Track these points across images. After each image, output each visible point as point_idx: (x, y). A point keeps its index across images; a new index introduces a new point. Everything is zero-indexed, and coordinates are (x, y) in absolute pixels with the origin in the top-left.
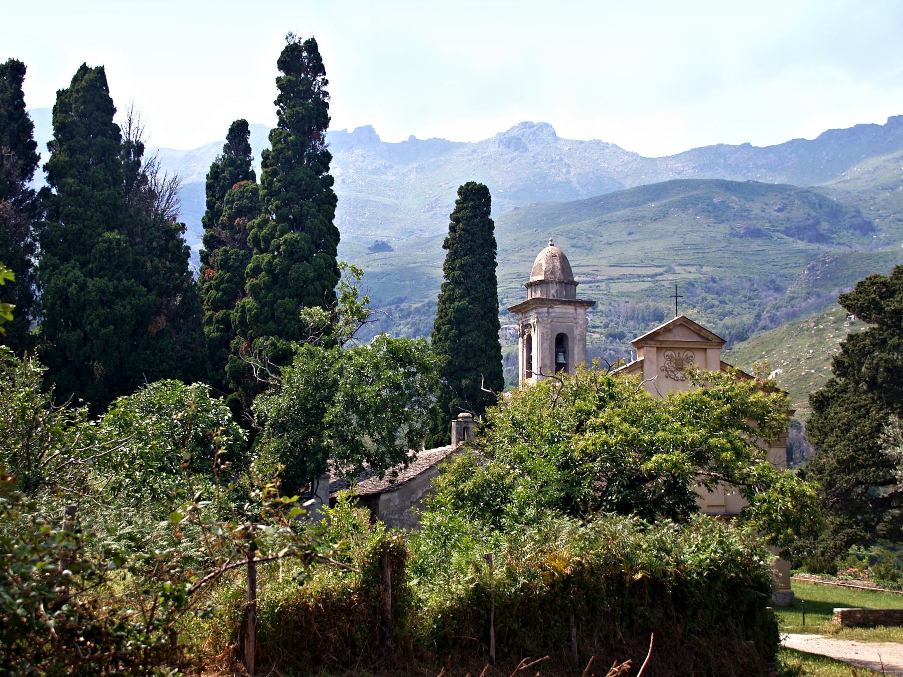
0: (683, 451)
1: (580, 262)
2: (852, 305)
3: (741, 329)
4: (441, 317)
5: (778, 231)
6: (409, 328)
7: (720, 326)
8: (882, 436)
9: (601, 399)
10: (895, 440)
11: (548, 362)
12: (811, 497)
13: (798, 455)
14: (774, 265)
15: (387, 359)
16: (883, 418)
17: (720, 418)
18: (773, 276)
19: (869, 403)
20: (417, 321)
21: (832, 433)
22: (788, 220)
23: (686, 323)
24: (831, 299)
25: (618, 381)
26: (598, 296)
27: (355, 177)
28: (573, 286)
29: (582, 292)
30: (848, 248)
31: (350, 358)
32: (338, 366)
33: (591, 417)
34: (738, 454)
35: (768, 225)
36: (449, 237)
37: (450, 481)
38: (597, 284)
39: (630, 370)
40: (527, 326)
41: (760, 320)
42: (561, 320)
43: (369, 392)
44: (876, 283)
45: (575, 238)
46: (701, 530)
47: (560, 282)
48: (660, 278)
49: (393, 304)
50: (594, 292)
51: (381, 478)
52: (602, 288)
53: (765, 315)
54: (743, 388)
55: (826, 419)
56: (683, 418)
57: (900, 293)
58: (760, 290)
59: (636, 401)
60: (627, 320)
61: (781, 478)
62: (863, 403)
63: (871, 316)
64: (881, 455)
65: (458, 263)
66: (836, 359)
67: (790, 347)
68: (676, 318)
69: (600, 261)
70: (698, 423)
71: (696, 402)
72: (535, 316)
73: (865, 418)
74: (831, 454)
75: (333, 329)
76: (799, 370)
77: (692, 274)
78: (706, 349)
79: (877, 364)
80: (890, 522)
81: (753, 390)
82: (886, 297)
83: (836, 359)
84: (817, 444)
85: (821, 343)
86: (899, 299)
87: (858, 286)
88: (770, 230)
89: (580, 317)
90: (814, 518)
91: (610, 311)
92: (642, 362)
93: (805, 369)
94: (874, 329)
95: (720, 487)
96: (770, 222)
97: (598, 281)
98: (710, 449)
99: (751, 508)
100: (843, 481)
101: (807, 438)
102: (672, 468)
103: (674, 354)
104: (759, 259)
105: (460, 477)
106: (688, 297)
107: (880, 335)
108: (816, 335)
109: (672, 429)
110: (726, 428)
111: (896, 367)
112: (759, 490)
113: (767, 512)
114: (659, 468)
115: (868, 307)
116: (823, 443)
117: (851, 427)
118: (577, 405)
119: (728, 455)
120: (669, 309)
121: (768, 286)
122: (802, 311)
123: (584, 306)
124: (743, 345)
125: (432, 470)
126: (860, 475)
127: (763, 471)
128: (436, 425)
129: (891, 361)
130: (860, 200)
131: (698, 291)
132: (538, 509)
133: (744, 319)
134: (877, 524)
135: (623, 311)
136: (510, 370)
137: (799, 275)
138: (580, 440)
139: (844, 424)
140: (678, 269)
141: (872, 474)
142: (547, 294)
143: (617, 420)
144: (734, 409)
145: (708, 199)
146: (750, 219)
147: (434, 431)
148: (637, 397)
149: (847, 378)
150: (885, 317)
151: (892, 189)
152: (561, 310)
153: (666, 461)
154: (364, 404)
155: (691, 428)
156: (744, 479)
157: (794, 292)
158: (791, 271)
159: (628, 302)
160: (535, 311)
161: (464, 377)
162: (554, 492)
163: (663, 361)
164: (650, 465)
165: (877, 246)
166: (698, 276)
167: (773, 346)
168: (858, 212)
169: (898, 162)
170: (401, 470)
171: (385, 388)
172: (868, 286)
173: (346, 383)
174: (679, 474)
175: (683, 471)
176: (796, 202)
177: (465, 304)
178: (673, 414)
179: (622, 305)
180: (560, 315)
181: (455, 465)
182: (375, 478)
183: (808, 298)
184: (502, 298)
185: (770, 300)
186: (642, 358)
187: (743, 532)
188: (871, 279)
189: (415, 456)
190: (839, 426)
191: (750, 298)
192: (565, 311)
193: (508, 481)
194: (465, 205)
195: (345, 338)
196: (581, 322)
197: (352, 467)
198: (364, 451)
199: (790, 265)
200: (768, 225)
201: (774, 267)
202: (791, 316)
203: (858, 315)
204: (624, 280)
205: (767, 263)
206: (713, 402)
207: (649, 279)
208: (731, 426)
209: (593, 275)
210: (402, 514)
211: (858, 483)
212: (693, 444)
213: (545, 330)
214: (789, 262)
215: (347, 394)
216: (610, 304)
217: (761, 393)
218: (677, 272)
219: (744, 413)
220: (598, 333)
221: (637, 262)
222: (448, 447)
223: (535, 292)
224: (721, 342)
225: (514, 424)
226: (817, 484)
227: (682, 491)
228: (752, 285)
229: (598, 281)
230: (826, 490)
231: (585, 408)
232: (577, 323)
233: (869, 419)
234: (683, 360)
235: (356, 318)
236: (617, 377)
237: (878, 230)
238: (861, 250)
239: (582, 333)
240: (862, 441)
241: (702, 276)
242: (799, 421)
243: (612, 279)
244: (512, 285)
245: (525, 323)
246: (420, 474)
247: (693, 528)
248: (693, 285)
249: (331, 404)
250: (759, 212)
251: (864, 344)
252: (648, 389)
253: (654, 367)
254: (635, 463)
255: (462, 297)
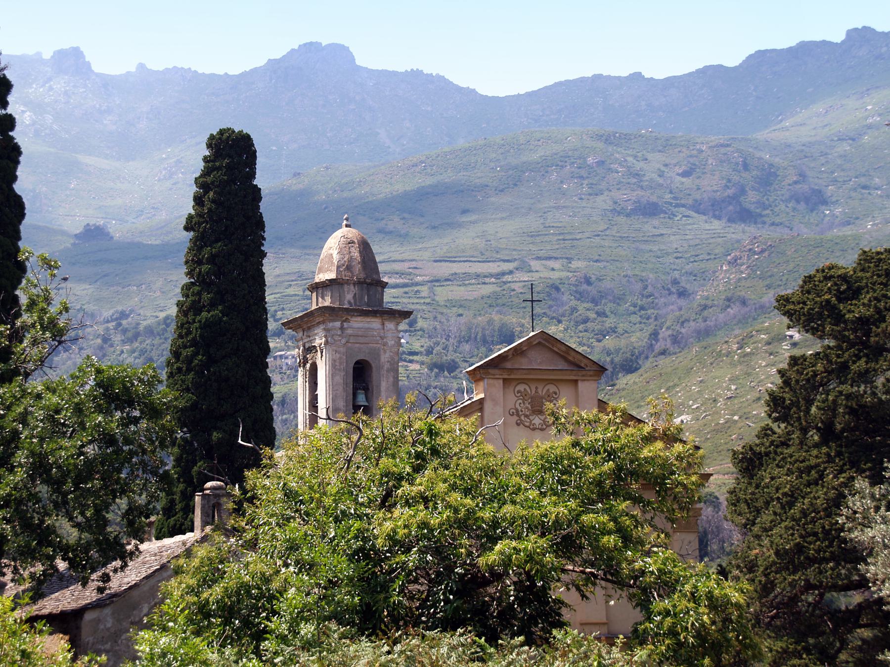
0: (543, 535)
1: (391, 254)
2: (796, 311)
3: (628, 355)
4: (180, 336)
5: (683, 206)
6: (135, 358)
7: (597, 350)
8: (845, 511)
9: (419, 456)
10: (864, 518)
11: (341, 404)
12: (738, 606)
13: (715, 547)
14: (677, 258)
15: (95, 397)
16: (845, 485)
17: (599, 483)
18: (676, 274)
19: (824, 462)
20: (148, 347)
21: (767, 509)
22: (699, 189)
23: (545, 342)
24: (762, 307)
25: (445, 427)
26: (418, 307)
27: (55, 127)
28: (379, 289)
29: (390, 298)
30: (787, 231)
31: (39, 397)
32: (20, 409)
33: (403, 483)
34: (627, 539)
35: (668, 197)
36: (193, 212)
37: (188, 587)
38: (416, 289)
39: (465, 412)
40: (310, 349)
41: (657, 341)
42: (362, 340)
43: (66, 449)
44: (832, 277)
45: (382, 219)
46: (571, 655)
47: (360, 283)
48: (508, 278)
49: (112, 321)
50: (412, 301)
51: (84, 585)
52: (423, 294)
53: (664, 333)
54: (632, 435)
55: (757, 487)
56: (542, 484)
57: (868, 292)
58: (657, 295)
59: (472, 457)
60: (460, 342)
61: (692, 576)
62: (813, 462)
63: (824, 328)
64: (845, 541)
65: (206, 252)
66: (771, 394)
67: (701, 382)
68: (532, 334)
69: (420, 253)
70: (565, 490)
71: (562, 458)
72: (322, 334)
73: (817, 484)
74: (766, 542)
75: (13, 353)
76: (716, 416)
77: (553, 272)
78: (576, 381)
79: (834, 401)
80: (860, 649)
81: (649, 439)
82: (847, 299)
83: (771, 394)
84: (745, 526)
85: (749, 374)
86: (866, 301)
87: (804, 282)
88: (671, 204)
89: (390, 335)
90: (745, 638)
91: (435, 329)
92: (481, 401)
93: (725, 414)
94: (829, 347)
95: (599, 592)
96: (671, 192)
97: (417, 284)
98: (584, 531)
99: (647, 624)
100: (784, 584)
101: (729, 517)
102: (526, 562)
103: (530, 389)
104: (655, 248)
105: (204, 579)
106: (550, 307)
107: (838, 356)
108: (740, 363)
109: (526, 500)
110: (608, 498)
111: (863, 406)
112: (659, 596)
113: (673, 633)
114: (507, 562)
115: (820, 314)
116: (754, 524)
117: (797, 499)
118: (381, 466)
119: (610, 540)
120: (523, 326)
121: (669, 290)
122: (718, 327)
123: (395, 317)
124: (631, 378)
125: (164, 571)
126: (811, 573)
127: (665, 564)
128: (172, 502)
129: (857, 397)
130: (806, 157)
131: (565, 298)
132: (319, 624)
133: (633, 339)
134: (839, 651)
135: (454, 329)
136: (286, 420)
137: (715, 272)
138: (385, 520)
139: (785, 494)
140: (535, 265)
141: (830, 572)
142: (340, 301)
143: (442, 487)
144: (619, 468)
145: (580, 158)
146: (642, 188)
147: (168, 511)
148: (472, 451)
149: (788, 423)
150: (845, 329)
151: (853, 140)
152: (360, 325)
153: (517, 551)
154: (59, 467)
155: (554, 498)
156: (636, 578)
157: (707, 298)
158: (703, 265)
159: (461, 315)
160: (322, 327)
161: (216, 428)
162: (347, 597)
163: (512, 400)
164: (492, 557)
165: (831, 227)
166: (564, 274)
167: (676, 380)
168: (803, 176)
169: (862, 98)
170: (115, 571)
171: (90, 442)
172: (820, 281)
173: (33, 437)
174: (537, 571)
175: (543, 566)
176: (710, 162)
177: (217, 315)
178: (528, 478)
179: (453, 320)
180: (360, 333)
181: (196, 562)
182: (78, 587)
183: (729, 306)
184: (276, 311)
185: (672, 311)
186: (482, 396)
187: (636, 658)
188: (823, 271)
189: (137, 549)
190: (778, 498)
191: (642, 308)
192: (366, 325)
193: (275, 585)
194: (217, 164)
195: (31, 366)
196: (391, 343)
197: (39, 568)
198: (60, 542)
199: (701, 257)
200: (668, 197)
201: (677, 261)
202: (703, 334)
203: (804, 327)
204: (455, 282)
205: (668, 254)
206: (587, 458)
207: (493, 280)
208: (616, 495)
209: (410, 274)
210: (116, 642)
211: (809, 587)
212: (557, 523)
213: (338, 355)
214: (699, 252)
215: (32, 454)
216: (435, 318)
217: (659, 445)
218: (533, 269)
219: (634, 474)
220: (417, 362)
221: (475, 254)
222: (189, 535)
223: (323, 298)
224: (600, 370)
225: (285, 495)
226: (746, 586)
227: (542, 595)
228: (645, 287)
229: (417, 284)
230: (760, 598)
231: (395, 469)
232: (385, 344)
233: (823, 487)
234: (542, 398)
235: (48, 334)
236: (443, 421)
237: (832, 203)
238: (807, 233)
239: (393, 359)
240: (813, 521)
241: (570, 275)
242: (717, 494)
243: (437, 281)
244: (291, 291)
245: (307, 346)
246: (147, 578)
247: (558, 654)
248: (557, 289)
249: (7, 469)
250: (655, 176)
251: (814, 371)
252: (488, 440)
253: (500, 409)
254: (469, 554)
255: (212, 305)
